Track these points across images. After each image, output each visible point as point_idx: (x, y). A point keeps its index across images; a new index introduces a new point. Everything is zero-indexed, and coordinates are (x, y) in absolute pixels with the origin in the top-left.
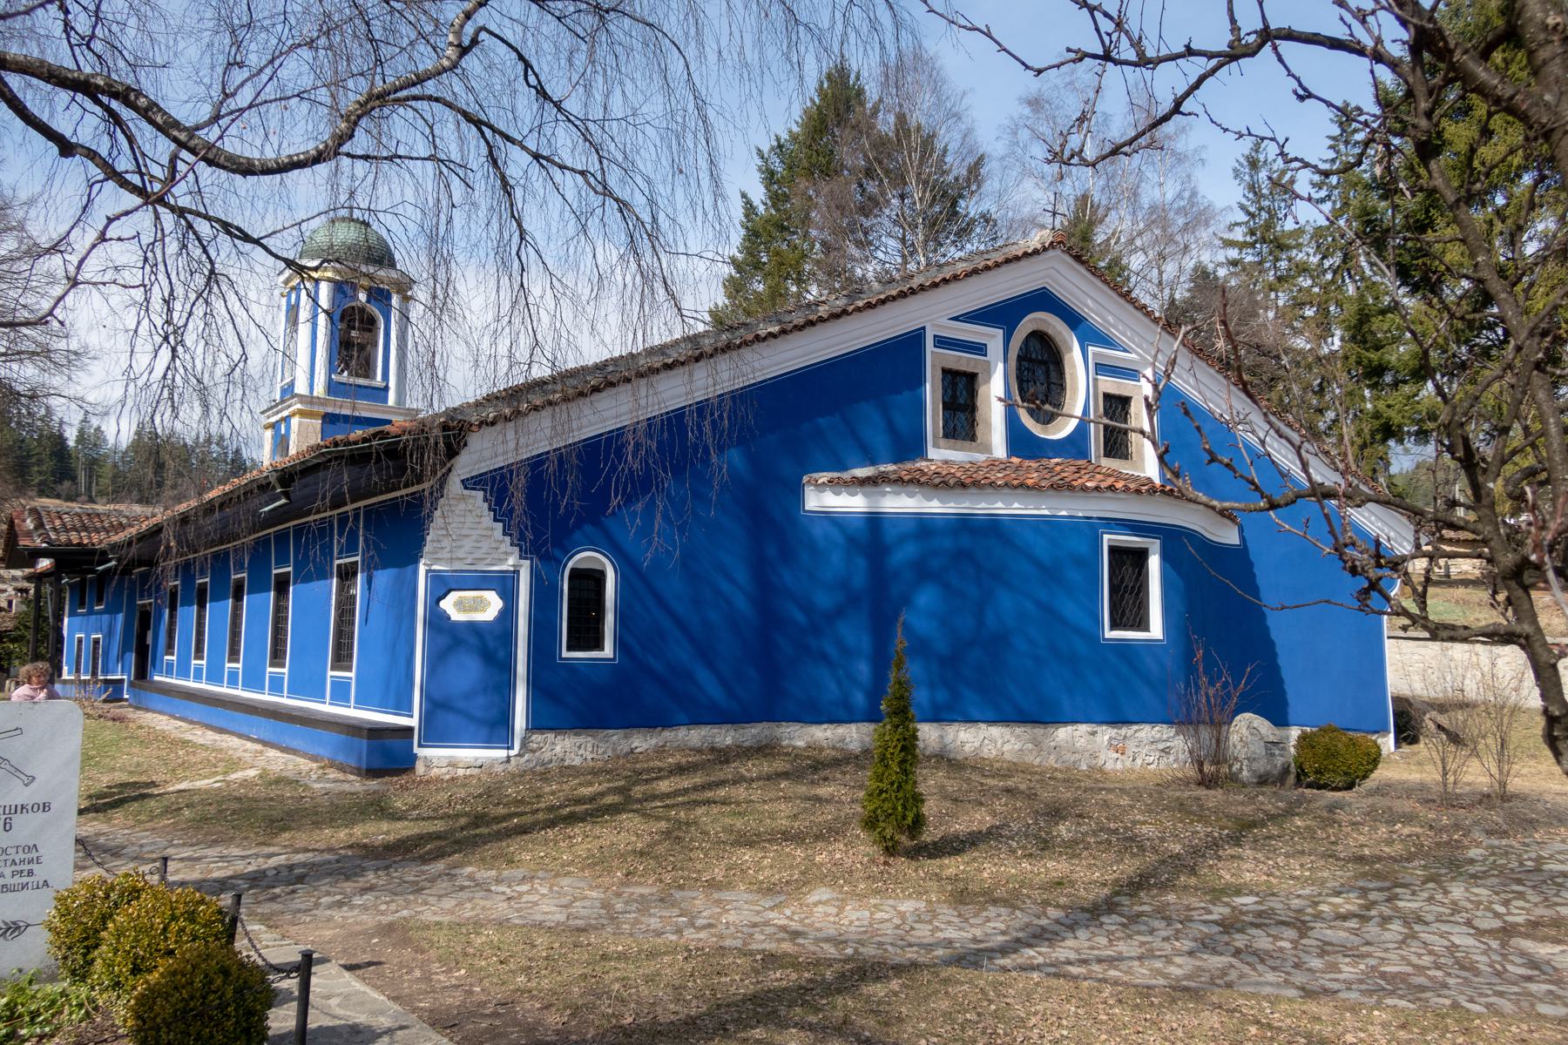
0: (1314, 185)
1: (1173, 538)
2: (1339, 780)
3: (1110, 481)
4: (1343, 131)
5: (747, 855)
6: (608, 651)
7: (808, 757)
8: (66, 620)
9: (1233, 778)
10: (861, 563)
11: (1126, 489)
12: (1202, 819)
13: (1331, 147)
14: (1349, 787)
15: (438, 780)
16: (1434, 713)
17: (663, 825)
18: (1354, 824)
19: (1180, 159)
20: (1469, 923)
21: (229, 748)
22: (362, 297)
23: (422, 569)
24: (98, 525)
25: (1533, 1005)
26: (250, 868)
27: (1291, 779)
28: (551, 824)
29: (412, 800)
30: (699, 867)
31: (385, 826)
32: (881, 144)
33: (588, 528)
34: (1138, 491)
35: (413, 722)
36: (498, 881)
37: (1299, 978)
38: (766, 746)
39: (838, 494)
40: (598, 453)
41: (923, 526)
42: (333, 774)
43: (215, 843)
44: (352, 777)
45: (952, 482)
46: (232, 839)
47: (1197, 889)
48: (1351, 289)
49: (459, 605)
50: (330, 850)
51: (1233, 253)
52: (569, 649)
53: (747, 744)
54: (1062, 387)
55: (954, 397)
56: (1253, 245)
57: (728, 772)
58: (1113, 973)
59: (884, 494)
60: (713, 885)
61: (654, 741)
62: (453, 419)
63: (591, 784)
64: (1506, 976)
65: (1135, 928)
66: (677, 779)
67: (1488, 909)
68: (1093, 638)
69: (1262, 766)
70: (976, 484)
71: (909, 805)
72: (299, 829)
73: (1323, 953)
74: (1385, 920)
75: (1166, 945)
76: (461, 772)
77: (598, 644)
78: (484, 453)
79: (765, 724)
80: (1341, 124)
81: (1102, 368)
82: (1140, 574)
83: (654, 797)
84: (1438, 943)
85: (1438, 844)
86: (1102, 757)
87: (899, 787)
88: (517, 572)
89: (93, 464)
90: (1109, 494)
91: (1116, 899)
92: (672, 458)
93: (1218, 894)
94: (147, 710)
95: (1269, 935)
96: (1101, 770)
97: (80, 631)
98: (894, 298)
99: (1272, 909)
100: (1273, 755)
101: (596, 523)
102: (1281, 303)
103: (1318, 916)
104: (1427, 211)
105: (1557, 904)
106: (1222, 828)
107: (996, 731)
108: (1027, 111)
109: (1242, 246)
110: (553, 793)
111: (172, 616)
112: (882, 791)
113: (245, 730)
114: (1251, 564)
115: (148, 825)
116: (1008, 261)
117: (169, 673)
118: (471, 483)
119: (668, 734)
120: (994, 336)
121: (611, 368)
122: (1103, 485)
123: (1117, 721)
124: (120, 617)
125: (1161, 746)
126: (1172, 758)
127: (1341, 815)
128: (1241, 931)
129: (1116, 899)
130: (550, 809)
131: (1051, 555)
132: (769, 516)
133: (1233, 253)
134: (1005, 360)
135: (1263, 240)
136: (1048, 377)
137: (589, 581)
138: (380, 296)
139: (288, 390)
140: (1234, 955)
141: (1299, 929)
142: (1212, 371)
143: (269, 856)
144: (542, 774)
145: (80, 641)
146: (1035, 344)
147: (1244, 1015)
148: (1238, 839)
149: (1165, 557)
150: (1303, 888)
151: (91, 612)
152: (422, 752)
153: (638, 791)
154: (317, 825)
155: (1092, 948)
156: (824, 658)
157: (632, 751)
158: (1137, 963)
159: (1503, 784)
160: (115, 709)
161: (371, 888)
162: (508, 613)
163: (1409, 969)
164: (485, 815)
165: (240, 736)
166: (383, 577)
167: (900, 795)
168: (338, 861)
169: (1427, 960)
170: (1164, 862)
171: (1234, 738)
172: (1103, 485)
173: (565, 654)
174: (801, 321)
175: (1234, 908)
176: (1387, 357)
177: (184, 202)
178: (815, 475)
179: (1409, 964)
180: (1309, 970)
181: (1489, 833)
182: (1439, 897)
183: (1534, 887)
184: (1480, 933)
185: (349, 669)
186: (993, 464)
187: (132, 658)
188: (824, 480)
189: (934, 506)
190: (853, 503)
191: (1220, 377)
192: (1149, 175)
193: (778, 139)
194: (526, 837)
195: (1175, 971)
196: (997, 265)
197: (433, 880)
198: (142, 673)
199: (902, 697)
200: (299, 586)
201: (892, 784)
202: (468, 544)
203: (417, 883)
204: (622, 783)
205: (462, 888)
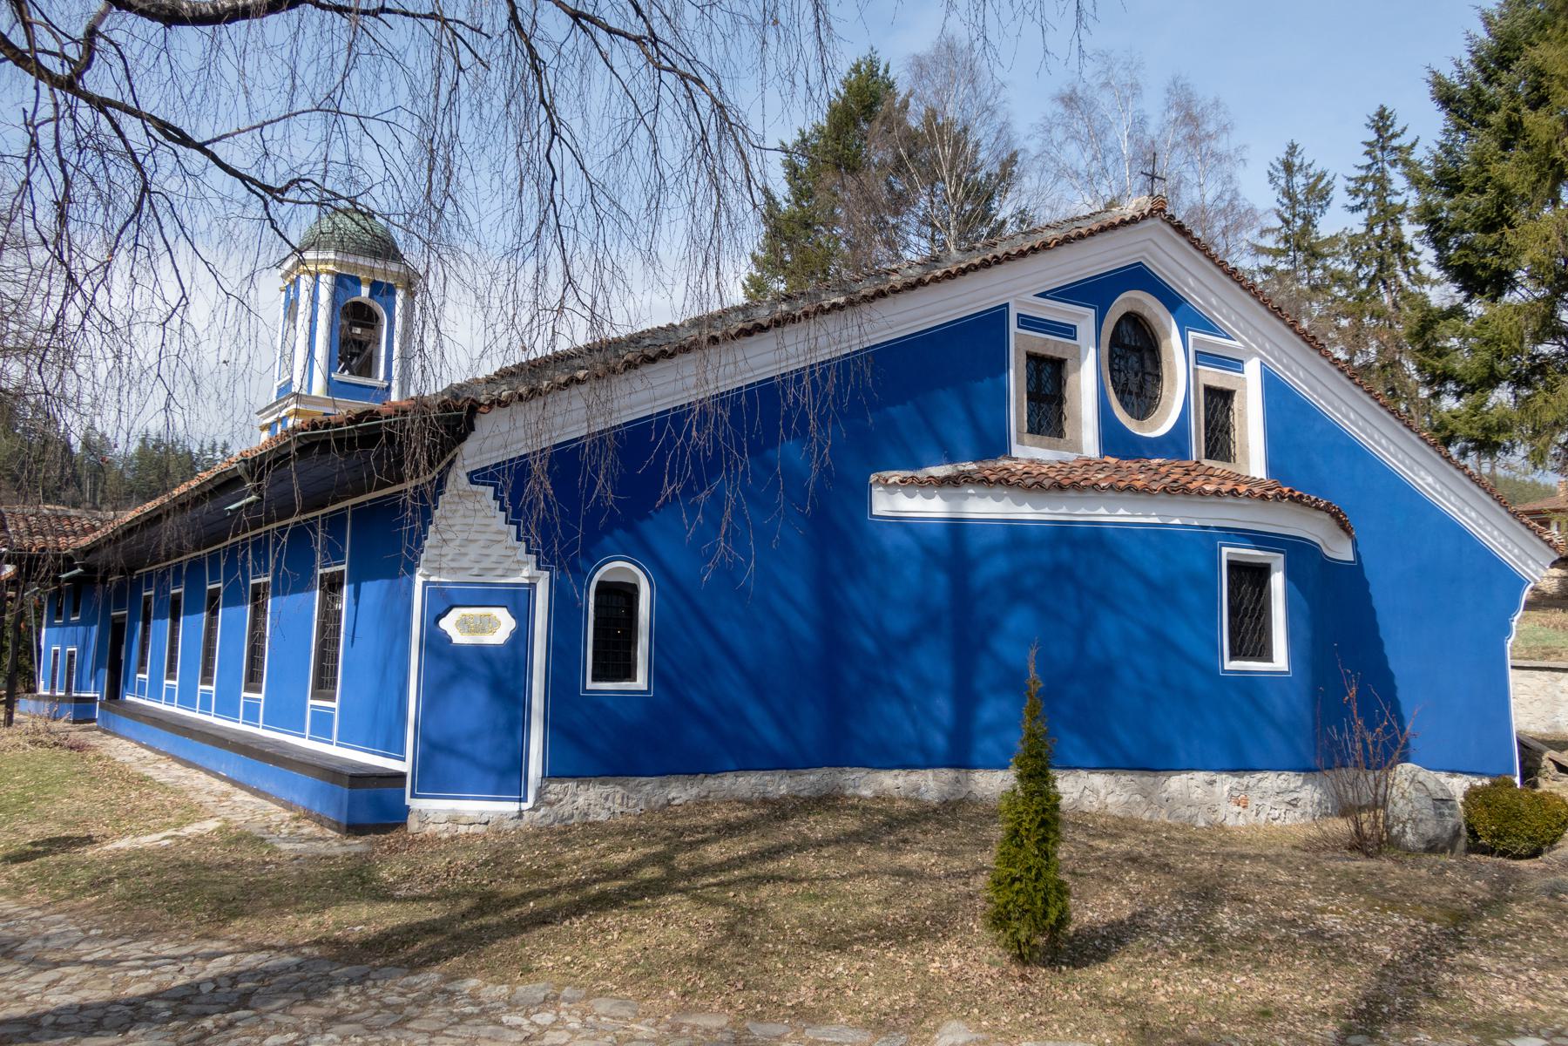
0: (1350, 192)
1: (1300, 553)
2: (1523, 846)
3: (1229, 486)
4: (1380, 136)
5: (840, 966)
6: (641, 682)
7: (879, 811)
8: (44, 630)
10: (941, 580)
12: (1393, 906)
13: (1367, 153)
14: (1535, 854)
15: (435, 839)
17: (721, 912)
19: (1219, 158)
21: (193, 788)
22: (365, 291)
23: (419, 580)
24: (68, 528)
26: (181, 980)
27: (1461, 845)
28: (577, 910)
29: (403, 869)
30: (779, 983)
31: (364, 911)
32: (912, 138)
33: (619, 533)
34: (1263, 497)
35: (405, 767)
36: (512, 1005)
38: (827, 796)
39: (911, 496)
40: (636, 440)
41: (1016, 535)
42: (309, 828)
43: (144, 934)
44: (330, 833)
45: (1047, 483)
46: (167, 928)
47: (1453, 1024)
48: (1387, 299)
49: (463, 624)
50: (292, 948)
51: (1266, 261)
52: (595, 678)
53: (805, 793)
54: (1159, 378)
55: (1039, 385)
56: (1284, 253)
57: (787, 832)
59: (968, 496)
60: (802, 1014)
61: (694, 791)
62: (457, 397)
63: (622, 848)
66: (728, 843)
68: (1211, 671)
69: (1430, 828)
70: (1075, 486)
71: (1051, 899)
72: (253, 914)
76: (462, 829)
77: (629, 674)
78: (496, 440)
79: (826, 770)
80: (1378, 130)
81: (1203, 357)
83: (705, 870)
86: (1222, 811)
87: (1039, 876)
88: (533, 586)
89: (100, 468)
90: (1230, 500)
92: (750, 432)
94: (115, 735)
96: (1221, 827)
97: (57, 644)
98: (976, 268)
100: (1442, 815)
101: (629, 528)
104: (1500, 208)
106: (1428, 920)
107: (1098, 780)
108: (1060, 109)
109: (1277, 253)
110: (578, 860)
111: (145, 630)
112: (1014, 880)
113: (212, 765)
114: (1366, 584)
115: (65, 905)
116: (1103, 229)
117: (141, 693)
118: (476, 477)
119: (711, 782)
120: (1085, 317)
121: (648, 342)
122: (1224, 489)
123: (1240, 767)
124: (95, 629)
130: (576, 886)
131: (1164, 570)
132: (836, 524)
133: (1266, 261)
134: (1098, 346)
136: (1142, 365)
137: (619, 598)
138: (382, 290)
139: (285, 390)
143: (210, 957)
144: (560, 833)
145: (56, 654)
146: (1127, 328)
149: (1290, 575)
151: (67, 624)
152: (416, 804)
153: (682, 860)
154: (278, 907)
156: (897, 692)
157: (669, 803)
160: (77, 734)
161: (337, 1018)
162: (521, 637)
164: (493, 895)
165: (208, 772)
166: (373, 590)
167: (1040, 885)
168: (299, 967)
172: (1224, 489)
173: (590, 685)
174: (870, 291)
176: (1452, 365)
177: (110, 93)
178: (885, 474)
185: (332, 698)
186: (1087, 463)
187: (104, 674)
188: (896, 479)
189: (1026, 511)
190: (931, 507)
192: (1188, 176)
193: (802, 133)
194: (546, 930)
196: (1092, 233)
197: (421, 1003)
198: (114, 692)
199: (1039, 755)
200: (286, 600)
201: (1029, 869)
202: (473, 551)
203: (401, 1007)
204: (660, 848)
205: (463, 1018)
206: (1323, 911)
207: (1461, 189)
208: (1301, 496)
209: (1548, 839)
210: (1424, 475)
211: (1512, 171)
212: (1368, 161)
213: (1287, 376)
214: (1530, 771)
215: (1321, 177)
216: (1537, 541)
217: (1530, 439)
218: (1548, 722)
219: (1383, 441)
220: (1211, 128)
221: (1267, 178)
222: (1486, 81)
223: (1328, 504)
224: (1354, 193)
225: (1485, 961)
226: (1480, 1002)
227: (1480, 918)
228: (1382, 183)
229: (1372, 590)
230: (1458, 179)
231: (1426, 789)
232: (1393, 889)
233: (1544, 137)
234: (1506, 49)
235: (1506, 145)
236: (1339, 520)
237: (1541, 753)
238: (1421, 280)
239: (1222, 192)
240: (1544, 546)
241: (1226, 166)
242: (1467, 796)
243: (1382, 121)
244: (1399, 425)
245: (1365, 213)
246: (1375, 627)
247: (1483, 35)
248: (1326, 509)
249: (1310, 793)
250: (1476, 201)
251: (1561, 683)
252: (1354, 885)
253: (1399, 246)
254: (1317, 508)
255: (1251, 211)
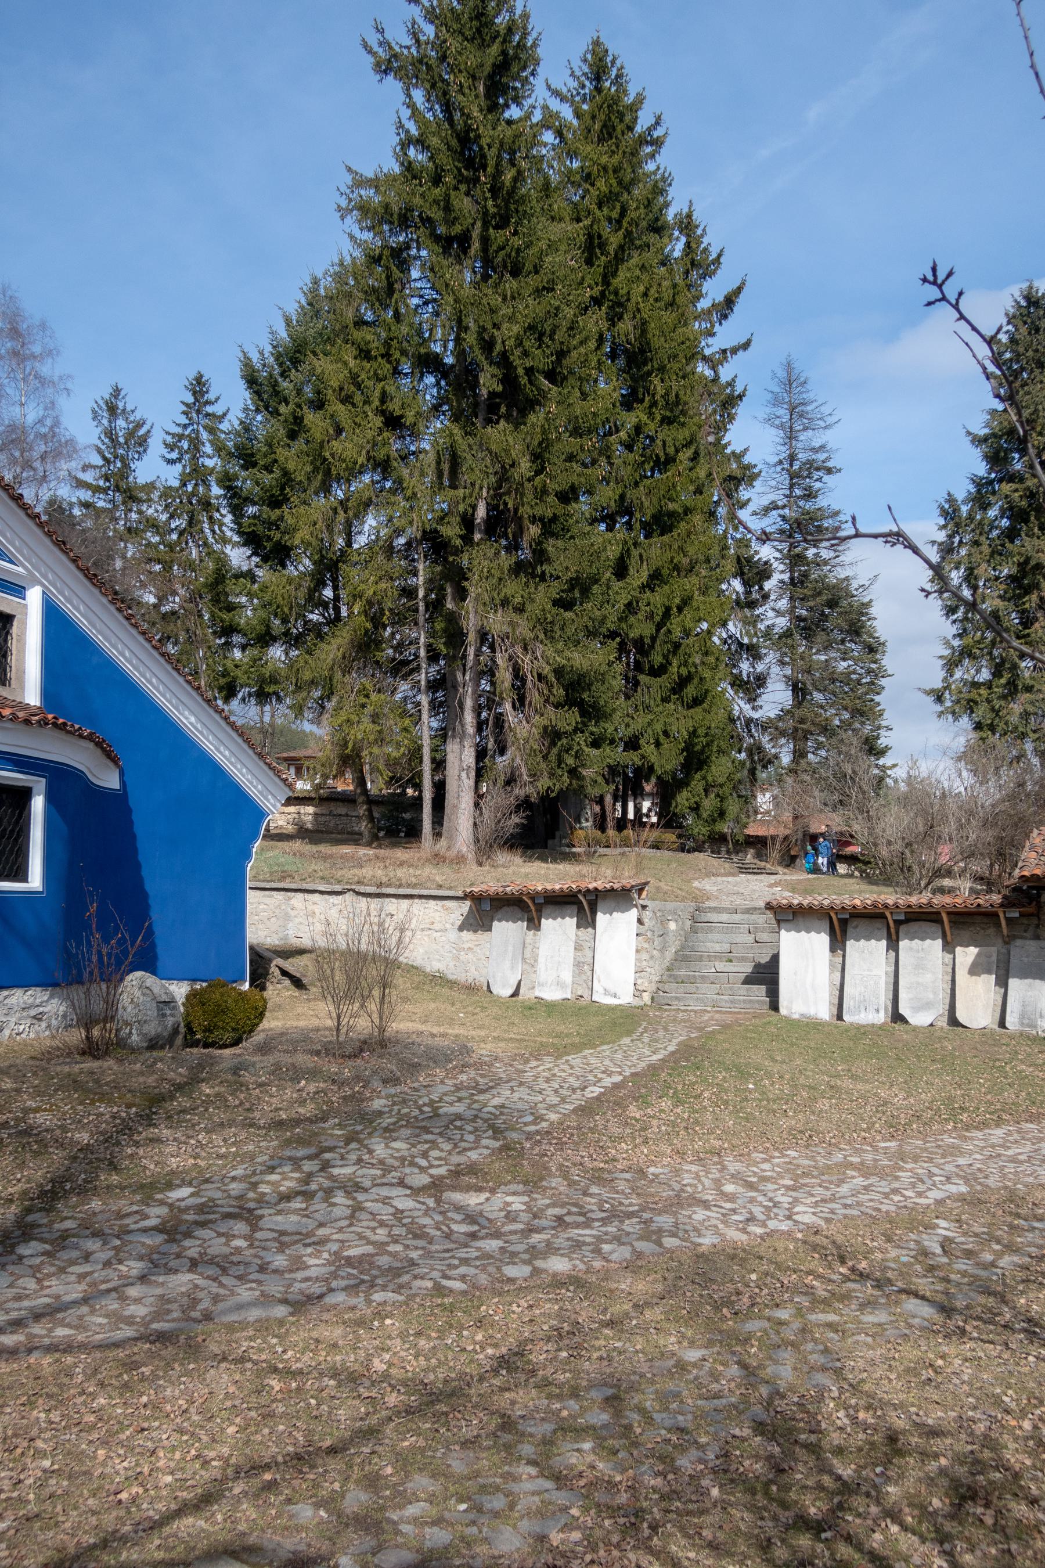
0: (167, 446)
1: (63, 781)
2: (228, 1037)
9: (122, 1043)
11: (14, 718)
12: (103, 1097)
13: (184, 413)
14: (236, 1042)
16: (279, 961)
18: (261, 1085)
19: (43, 381)
20: (401, 1183)
25: (499, 1269)
27: (179, 1040)
34: (27, 722)
37: (275, 1287)
47: (123, 1189)
51: (85, 495)
56: (105, 491)
58: (61, 1332)
64: (455, 1237)
65: (65, 1255)
67: (413, 1164)
69: (152, 1029)
73: (282, 1247)
74: (329, 1192)
75: (109, 1272)
80: (194, 393)
82: (20, 816)
84: (385, 1213)
85: (344, 1098)
91: (30, 1218)
93: (149, 1190)
95: (220, 1235)
99: (213, 1200)
100: (164, 1015)
102: (129, 554)
103: (261, 1200)
104: (283, 489)
105: (465, 1150)
106: (129, 1106)
109: (96, 490)
114: (130, 811)
125: (33, 1012)
126: (44, 1025)
127: (247, 1077)
128: (188, 1235)
129: (30, 1218)
133: (85, 495)
135: (117, 489)
140: (190, 1271)
141: (247, 1220)
142: (104, 600)
147: (255, 1363)
148: (149, 1118)
149: (50, 799)
150: (234, 1168)
155: (18, 1298)
158: (85, 1309)
159: (382, 1030)
163: (369, 1249)
169: (382, 1234)
170: (74, 1158)
171: (125, 999)
175: (171, 1206)
179: (369, 1242)
180: (275, 1271)
181: (385, 1082)
182: (366, 1157)
183: (440, 1134)
184: (416, 1192)
191: (112, 608)
195: (139, 1311)
206: (37, 1110)
207: (254, 465)
208: (65, 724)
209: (247, 1029)
210: (190, 718)
211: (292, 458)
212: (184, 420)
213: (68, 608)
214: (259, 978)
215: (139, 425)
216: (277, 780)
217: (294, 692)
218: (281, 935)
219: (154, 680)
220: (37, 349)
221: (90, 415)
222: (282, 375)
223: (91, 734)
224: (171, 447)
225: (166, 1132)
226: (152, 1167)
227: (172, 1098)
228: (196, 444)
229: (134, 817)
230: (252, 455)
231: (149, 996)
232: (107, 1084)
233: (318, 437)
234: (299, 352)
235: (292, 435)
236: (103, 750)
237: (270, 961)
238: (225, 541)
239: (44, 417)
240: (281, 784)
241: (50, 391)
242: (188, 997)
243: (199, 386)
244: (169, 668)
245: (179, 467)
246: (135, 851)
247: (284, 334)
248: (90, 738)
249: (54, 1006)
250: (267, 479)
251: (292, 902)
252: (75, 1083)
253: (206, 505)
254: (81, 736)
255: (71, 442)
